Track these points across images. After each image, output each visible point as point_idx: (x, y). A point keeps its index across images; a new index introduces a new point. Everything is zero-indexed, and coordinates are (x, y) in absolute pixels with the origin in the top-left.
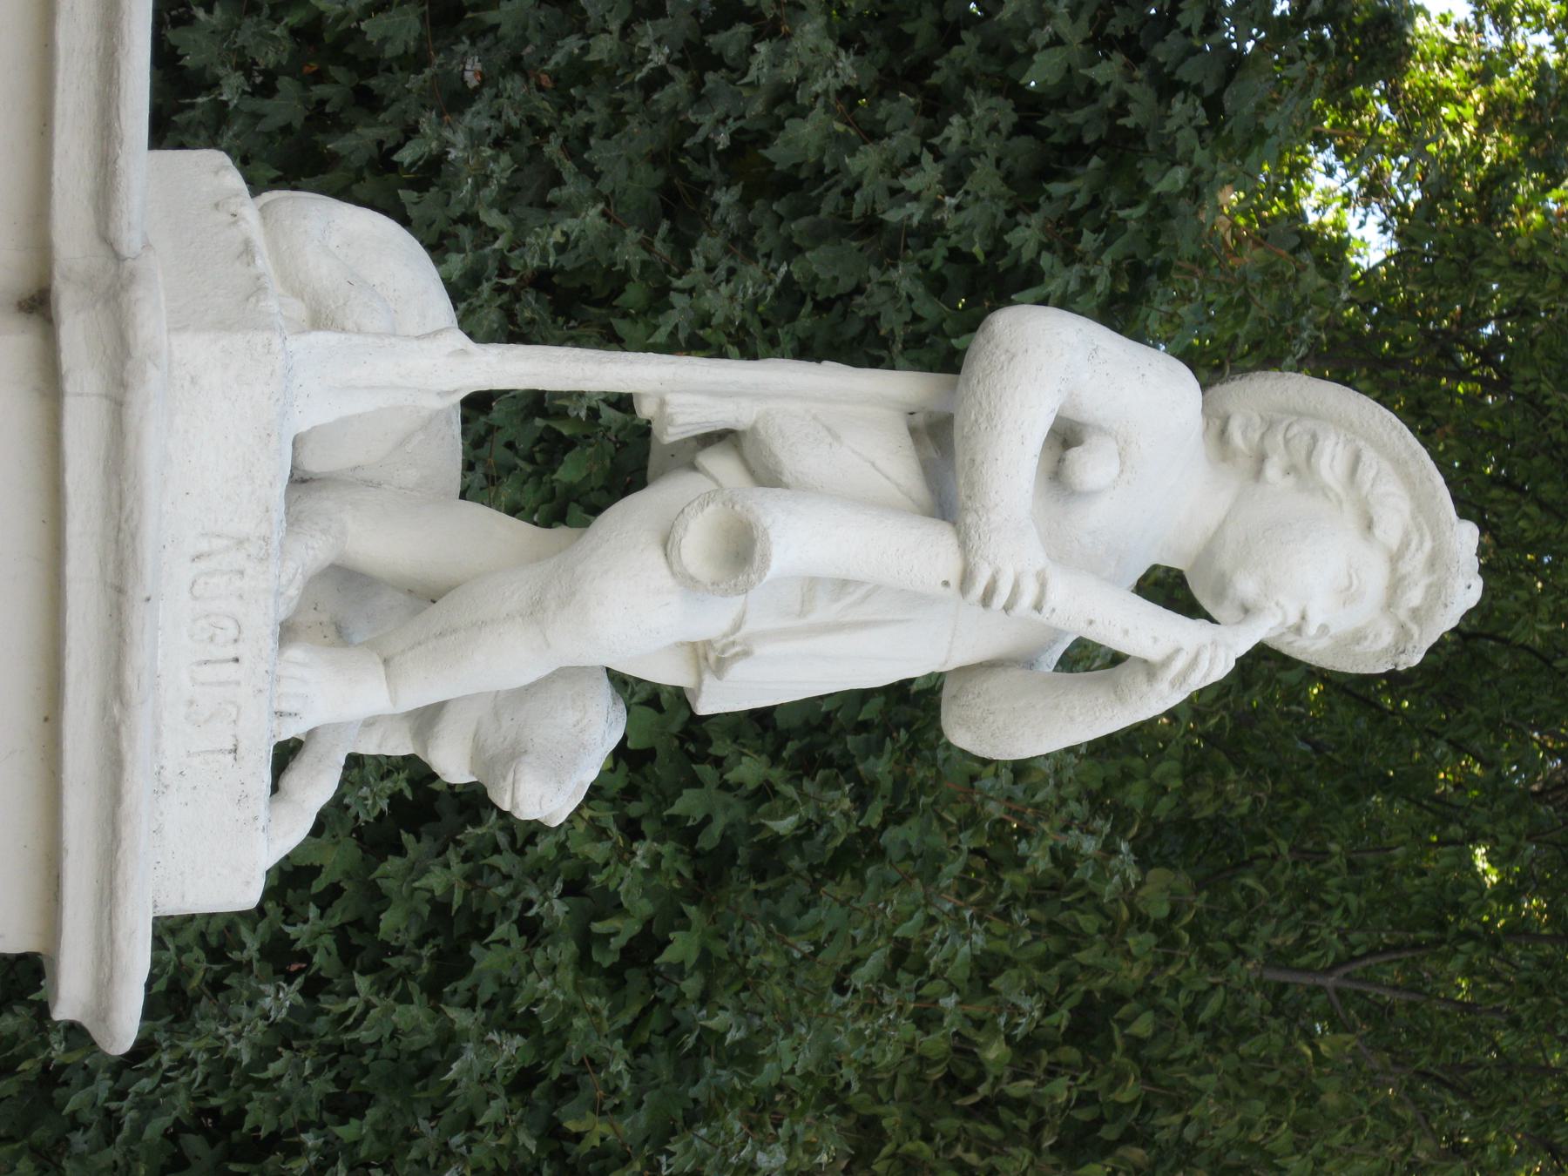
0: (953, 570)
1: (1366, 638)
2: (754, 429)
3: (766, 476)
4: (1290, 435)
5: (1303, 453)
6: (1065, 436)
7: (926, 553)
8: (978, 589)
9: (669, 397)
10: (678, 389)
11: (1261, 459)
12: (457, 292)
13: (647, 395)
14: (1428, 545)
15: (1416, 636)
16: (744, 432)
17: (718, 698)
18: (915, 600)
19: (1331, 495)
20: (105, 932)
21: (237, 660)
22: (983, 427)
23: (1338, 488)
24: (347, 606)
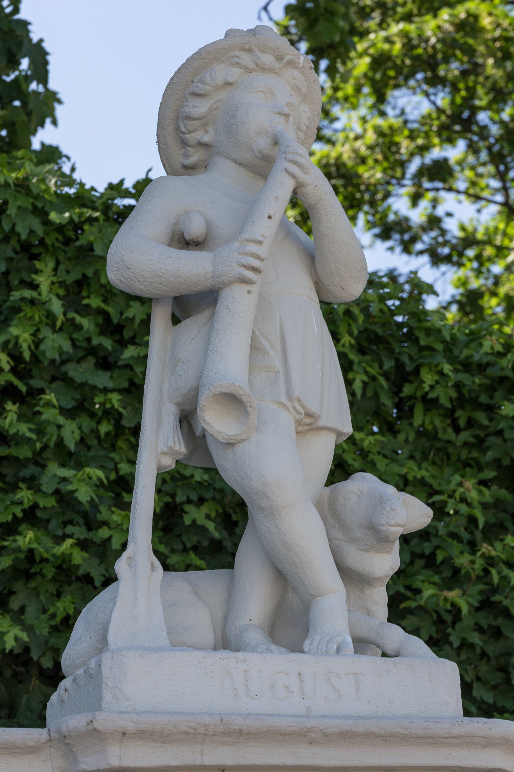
0: (244, 288)
1: (296, 84)
2: (178, 404)
3: (195, 394)
4: (186, 132)
5: (195, 122)
6: (184, 242)
7: (238, 308)
8: (249, 274)
9: (159, 451)
10: (157, 448)
11: (202, 145)
12: (375, 656)
13: (159, 462)
14: (237, 53)
15: (291, 57)
16: (182, 411)
17: (338, 416)
18: (263, 308)
19: (215, 106)
20: (455, 741)
21: (299, 674)
22: (164, 280)
23: (211, 102)
24: (291, 623)
